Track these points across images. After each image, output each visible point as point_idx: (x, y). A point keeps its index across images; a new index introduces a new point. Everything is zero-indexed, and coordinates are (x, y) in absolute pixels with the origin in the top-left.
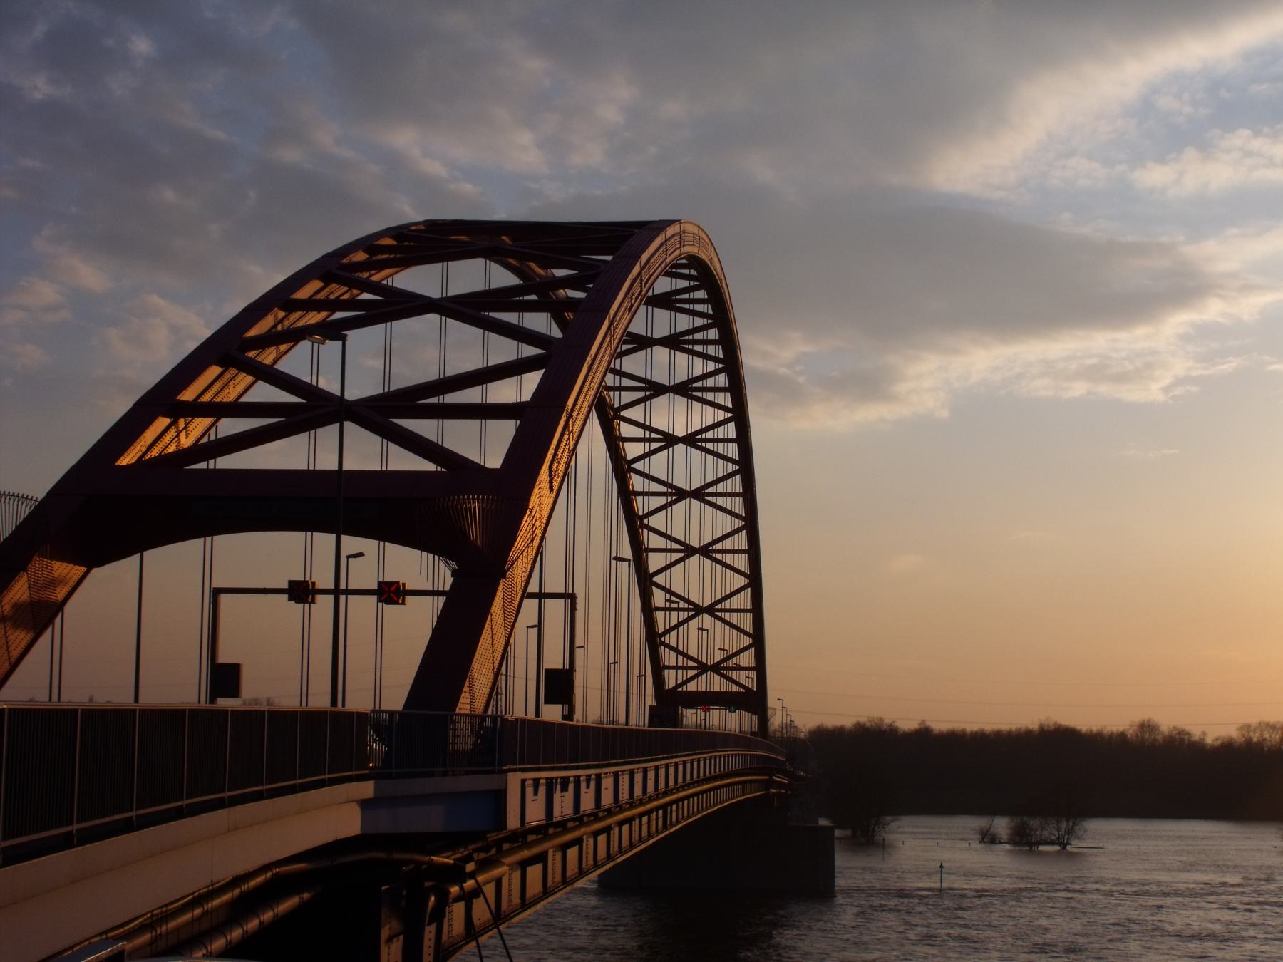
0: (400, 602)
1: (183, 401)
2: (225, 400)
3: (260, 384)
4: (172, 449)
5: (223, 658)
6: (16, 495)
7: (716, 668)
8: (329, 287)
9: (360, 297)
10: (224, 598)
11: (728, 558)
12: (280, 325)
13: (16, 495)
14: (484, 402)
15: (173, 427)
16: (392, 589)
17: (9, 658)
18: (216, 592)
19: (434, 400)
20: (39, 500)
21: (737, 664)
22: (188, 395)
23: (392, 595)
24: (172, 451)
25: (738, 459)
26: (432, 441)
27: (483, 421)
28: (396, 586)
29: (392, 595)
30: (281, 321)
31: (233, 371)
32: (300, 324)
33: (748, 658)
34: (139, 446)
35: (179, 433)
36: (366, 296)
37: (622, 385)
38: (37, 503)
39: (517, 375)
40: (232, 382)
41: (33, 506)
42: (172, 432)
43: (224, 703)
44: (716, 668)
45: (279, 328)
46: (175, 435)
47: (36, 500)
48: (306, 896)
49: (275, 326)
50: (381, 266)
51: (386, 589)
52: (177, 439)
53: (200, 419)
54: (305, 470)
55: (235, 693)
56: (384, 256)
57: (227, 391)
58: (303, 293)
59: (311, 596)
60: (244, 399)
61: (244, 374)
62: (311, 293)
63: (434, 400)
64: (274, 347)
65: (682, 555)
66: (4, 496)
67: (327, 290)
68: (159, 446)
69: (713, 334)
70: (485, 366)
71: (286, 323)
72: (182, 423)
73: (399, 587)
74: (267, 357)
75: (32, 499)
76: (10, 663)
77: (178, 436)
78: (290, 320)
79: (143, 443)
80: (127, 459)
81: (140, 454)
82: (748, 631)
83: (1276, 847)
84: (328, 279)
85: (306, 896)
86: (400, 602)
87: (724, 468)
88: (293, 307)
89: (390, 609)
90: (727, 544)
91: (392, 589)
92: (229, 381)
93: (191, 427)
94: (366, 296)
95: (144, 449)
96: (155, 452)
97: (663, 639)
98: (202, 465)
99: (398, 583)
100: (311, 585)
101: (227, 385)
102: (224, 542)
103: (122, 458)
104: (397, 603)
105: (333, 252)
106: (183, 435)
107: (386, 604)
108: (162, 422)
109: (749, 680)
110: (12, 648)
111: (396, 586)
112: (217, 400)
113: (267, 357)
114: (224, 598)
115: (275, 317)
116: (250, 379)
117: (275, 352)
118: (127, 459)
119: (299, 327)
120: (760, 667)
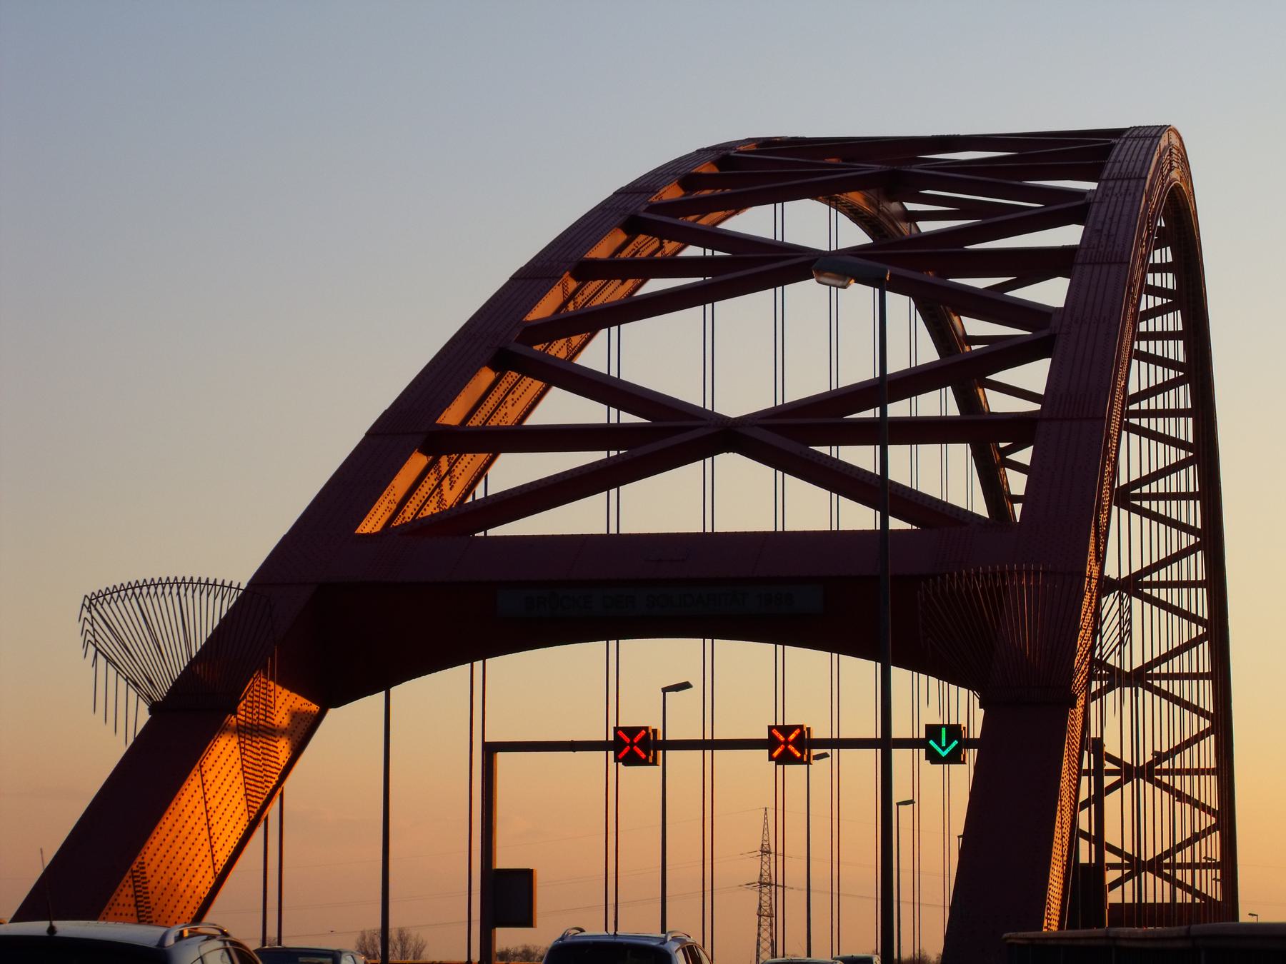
0: (651, 760)
3: (555, 392)
4: (431, 509)
6: (195, 580)
7: (1156, 866)
8: (635, 242)
9: (684, 254)
10: (502, 758)
11: (1173, 597)
12: (572, 302)
14: (944, 414)
15: (433, 471)
17: (214, 864)
18: (490, 750)
19: (628, 418)
20: (243, 586)
22: (452, 416)
23: (791, 748)
25: (1206, 617)
28: (797, 732)
29: (791, 748)
30: (572, 297)
31: (513, 376)
32: (598, 301)
33: (1212, 847)
34: (387, 501)
35: (440, 481)
36: (693, 251)
38: (241, 592)
40: (510, 396)
41: (234, 600)
42: (431, 480)
44: (1156, 866)
45: (571, 307)
46: (435, 483)
47: (238, 588)
48: (914, 527)
49: (565, 304)
51: (782, 738)
52: (437, 490)
53: (469, 456)
55: (525, 919)
56: (707, 192)
57: (503, 411)
58: (601, 251)
59: (806, 750)
60: (530, 421)
61: (529, 380)
63: (628, 418)
65: (1116, 778)
66: (168, 586)
67: (631, 247)
68: (411, 506)
69: (1173, 321)
70: (913, 365)
71: (580, 299)
72: (444, 461)
73: (647, 735)
74: (558, 349)
75: (215, 584)
76: (215, 873)
77: (439, 485)
79: (391, 497)
80: (372, 524)
81: (388, 515)
82: (1192, 524)
83: (187, 945)
84: (633, 226)
86: (651, 760)
88: (587, 271)
89: (795, 772)
92: (506, 396)
93: (457, 471)
94: (693, 251)
95: (394, 507)
96: (409, 513)
97: (1214, 822)
98: (717, 253)
99: (646, 728)
100: (652, 734)
101: (502, 401)
103: (363, 524)
104: (645, 763)
105: (628, 186)
106: (446, 483)
107: (625, 764)
108: (418, 462)
109: (1209, 884)
110: (217, 847)
111: (797, 732)
112: (493, 423)
115: (565, 290)
116: (538, 385)
117: (565, 347)
118: (372, 524)
119: (596, 306)
120: (1228, 865)
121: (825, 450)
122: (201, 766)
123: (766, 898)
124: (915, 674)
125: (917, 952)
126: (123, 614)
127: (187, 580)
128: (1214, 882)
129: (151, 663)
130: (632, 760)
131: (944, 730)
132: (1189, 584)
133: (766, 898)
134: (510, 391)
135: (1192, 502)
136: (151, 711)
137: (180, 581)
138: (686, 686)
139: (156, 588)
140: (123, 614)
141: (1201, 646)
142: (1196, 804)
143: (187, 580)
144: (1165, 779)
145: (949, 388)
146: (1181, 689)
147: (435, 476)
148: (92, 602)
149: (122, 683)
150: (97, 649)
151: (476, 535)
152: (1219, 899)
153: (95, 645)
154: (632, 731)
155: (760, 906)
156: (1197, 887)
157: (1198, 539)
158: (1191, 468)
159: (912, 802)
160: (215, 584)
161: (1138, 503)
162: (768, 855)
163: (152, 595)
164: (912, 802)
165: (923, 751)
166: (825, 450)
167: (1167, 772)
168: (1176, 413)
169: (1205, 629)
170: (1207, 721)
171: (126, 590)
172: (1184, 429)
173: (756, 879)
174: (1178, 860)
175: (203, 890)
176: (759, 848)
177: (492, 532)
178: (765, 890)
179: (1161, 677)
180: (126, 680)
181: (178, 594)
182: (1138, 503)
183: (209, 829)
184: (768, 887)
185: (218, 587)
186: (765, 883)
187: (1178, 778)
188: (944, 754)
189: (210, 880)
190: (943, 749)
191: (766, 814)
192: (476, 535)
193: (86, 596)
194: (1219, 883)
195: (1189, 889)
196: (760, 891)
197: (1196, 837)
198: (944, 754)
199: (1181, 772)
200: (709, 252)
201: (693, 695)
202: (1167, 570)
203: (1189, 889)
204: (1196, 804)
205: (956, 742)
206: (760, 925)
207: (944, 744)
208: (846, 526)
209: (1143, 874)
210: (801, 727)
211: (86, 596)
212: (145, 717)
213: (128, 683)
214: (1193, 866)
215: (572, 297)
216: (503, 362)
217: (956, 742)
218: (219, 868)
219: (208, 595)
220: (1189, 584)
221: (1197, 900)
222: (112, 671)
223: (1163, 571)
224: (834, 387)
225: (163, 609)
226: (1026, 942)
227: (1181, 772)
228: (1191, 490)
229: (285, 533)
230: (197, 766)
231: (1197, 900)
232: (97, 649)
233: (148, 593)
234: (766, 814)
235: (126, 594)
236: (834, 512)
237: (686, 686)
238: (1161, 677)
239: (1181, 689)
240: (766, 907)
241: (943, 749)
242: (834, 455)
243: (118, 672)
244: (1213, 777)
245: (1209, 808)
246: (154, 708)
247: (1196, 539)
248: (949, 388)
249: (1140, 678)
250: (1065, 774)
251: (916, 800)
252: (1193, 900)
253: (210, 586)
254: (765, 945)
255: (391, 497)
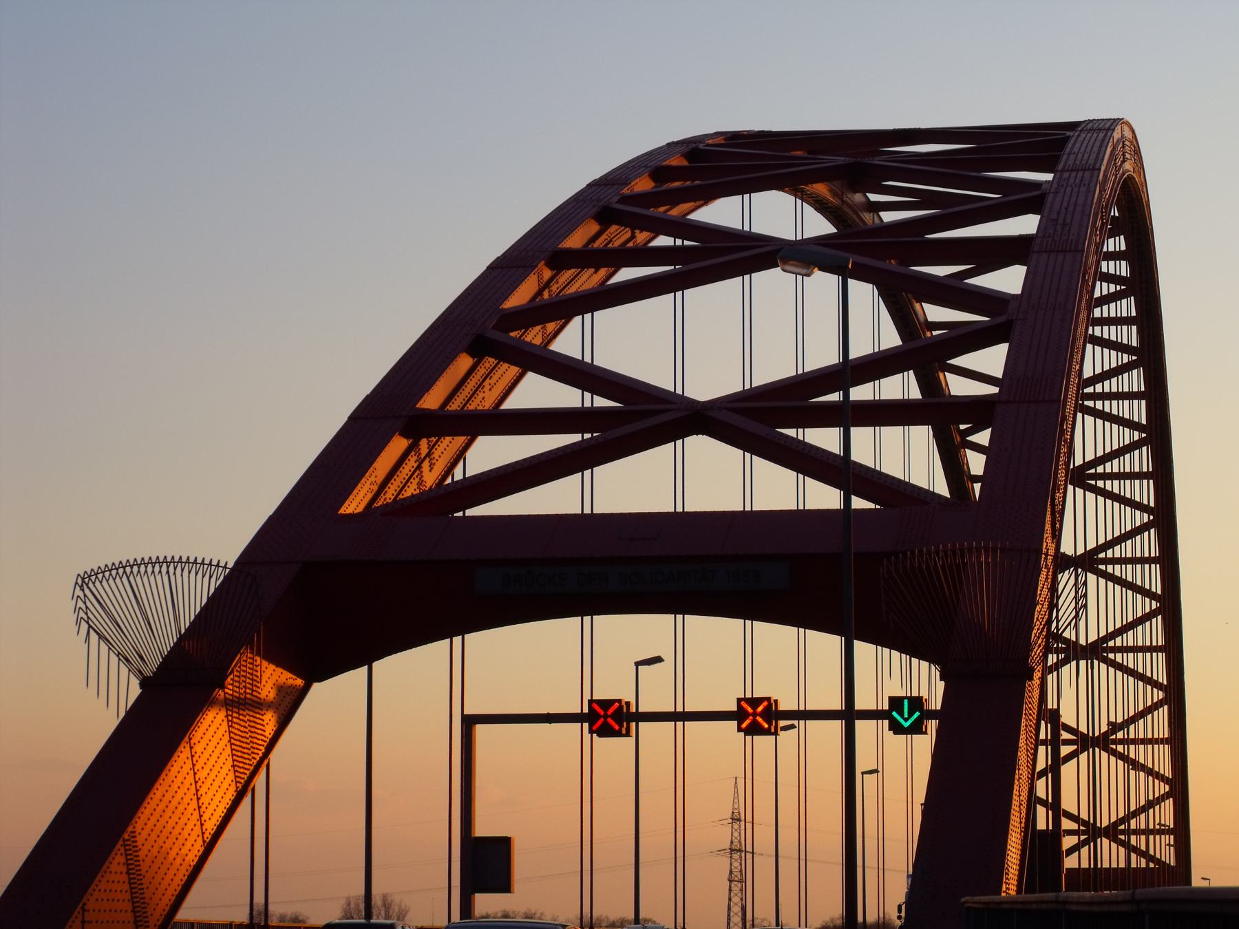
1: (424, 410)
2: (480, 408)
3: (531, 377)
4: (411, 490)
5: (482, 829)
7: (1112, 832)
10: (480, 730)
11: (1127, 572)
13: (184, 560)
15: (413, 453)
16: (610, 711)
18: (470, 722)
19: (601, 402)
20: (230, 565)
21: (1164, 825)
22: (431, 401)
23: (759, 719)
24: (409, 494)
25: (1159, 592)
26: (830, 453)
27: (587, 511)
28: (765, 704)
29: (759, 719)
30: (547, 285)
32: (572, 290)
33: (1165, 814)
34: (369, 482)
36: (663, 241)
37: (753, 509)
38: (228, 570)
39: (582, 470)
40: (488, 381)
42: (411, 462)
43: (487, 904)
44: (1112, 832)
45: (546, 295)
46: (415, 465)
47: (225, 567)
48: (878, 507)
49: (540, 292)
50: (676, 198)
51: (750, 710)
52: (418, 472)
53: (448, 439)
54: (795, 510)
55: (504, 885)
56: (677, 184)
57: (481, 395)
58: (575, 241)
60: (509, 404)
61: (506, 365)
62: (585, 241)
63: (601, 402)
64: (539, 327)
67: (604, 236)
69: (1127, 307)
71: (554, 288)
72: (424, 445)
74: (534, 336)
75: (203, 563)
76: (204, 842)
77: (419, 467)
78: (560, 284)
79: (373, 479)
80: (354, 504)
82: (1145, 502)
84: (606, 217)
85: (878, 507)
86: (773, 730)
87: (1120, 436)
88: (561, 260)
89: (604, 744)
90: (1126, 549)
91: (610, 711)
93: (436, 454)
94: (663, 241)
95: (375, 488)
98: (687, 243)
99: (619, 701)
100: (625, 706)
101: (480, 386)
102: (481, 643)
104: (618, 734)
105: (601, 178)
106: (426, 465)
107: (600, 735)
108: (399, 444)
110: (205, 817)
111: (765, 704)
112: (471, 407)
113: (534, 336)
114: (480, 730)
115: (540, 278)
116: (514, 370)
117: (540, 334)
118: (354, 504)
120: (1181, 831)
121: (791, 432)
122: (190, 739)
123: (736, 864)
124: (879, 648)
125: (881, 915)
126: (114, 592)
127: (176, 560)
128: (1167, 847)
129: (131, 637)
130: (753, 730)
131: (906, 702)
132: (1142, 561)
133: (736, 864)
134: (487, 376)
135: (1145, 482)
136: (142, 685)
137: (169, 560)
138: (658, 660)
139: (146, 567)
140: (114, 592)
141: (1154, 620)
142: (1150, 772)
143: (176, 560)
144: (1120, 748)
145: (911, 372)
146: (1135, 661)
147: (416, 458)
148: (84, 581)
149: (114, 659)
150: (90, 626)
151: (455, 515)
152: (1172, 864)
153: (88, 622)
154: (605, 704)
155: (731, 872)
156: (1151, 852)
157: (1152, 517)
158: (1144, 449)
159: (876, 771)
160: (203, 563)
161: (1093, 482)
162: (738, 823)
163: (142, 574)
164: (876, 771)
165: (886, 722)
166: (791, 432)
167: (1122, 742)
168: (1130, 396)
169: (1158, 604)
170: (1161, 693)
171: (117, 569)
172: (1138, 411)
173: (727, 845)
174: (1133, 826)
175: (192, 858)
176: (729, 815)
177: (470, 512)
178: (736, 856)
179: (1115, 650)
180: (118, 656)
181: (168, 572)
182: (1093, 482)
183: (198, 799)
184: (739, 853)
185: (206, 566)
186: (736, 850)
187: (1132, 747)
188: (906, 725)
189: (199, 848)
190: (906, 720)
191: (736, 783)
192: (455, 515)
193: (79, 575)
194: (1172, 848)
195: (1144, 854)
196: (731, 857)
197: (1150, 804)
198: (906, 725)
199: (1135, 742)
200: (679, 242)
201: (665, 668)
202: (1121, 546)
203: (1144, 854)
204: (1150, 772)
205: (917, 714)
206: (730, 890)
207: (906, 715)
208: (812, 505)
209: (1099, 840)
210: (768, 699)
211: (79, 575)
212: (136, 691)
213: (120, 659)
214: (1147, 832)
215: (547, 285)
216: (480, 348)
217: (917, 714)
218: (208, 836)
219: (190, 572)
220: (1142, 561)
221: (1152, 865)
222: (104, 647)
223: (1117, 548)
224: (800, 372)
225: (153, 587)
226: (981, 906)
227: (1135, 742)
228: (1145, 470)
229: (271, 514)
230: (186, 739)
231: (1152, 865)
232: (90, 626)
233: (139, 572)
234: (736, 783)
235: (117, 573)
236: (800, 492)
237: (658, 660)
238: (1115, 650)
239: (1135, 661)
240: (736, 872)
241: (906, 720)
242: (800, 437)
243: (110, 648)
244: (1166, 746)
245: (1163, 776)
246: (145, 683)
247: (1142, 518)
248: (911, 372)
249: (1096, 651)
250: (1022, 744)
251: (880, 769)
252: (1148, 864)
253: (198, 565)
254: (736, 909)
255: (373, 479)
